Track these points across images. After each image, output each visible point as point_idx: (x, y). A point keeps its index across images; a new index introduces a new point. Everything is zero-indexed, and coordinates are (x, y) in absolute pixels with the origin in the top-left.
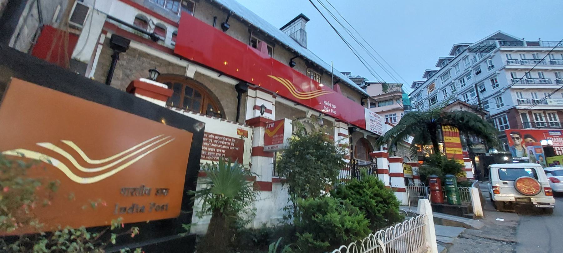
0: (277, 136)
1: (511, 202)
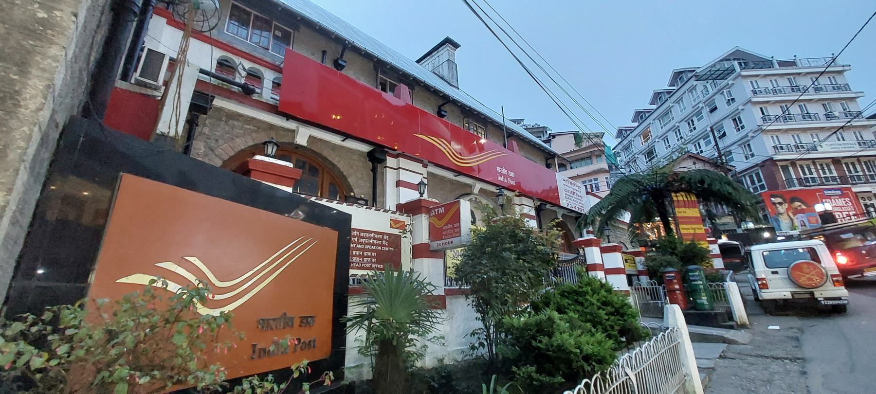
0: (450, 226)
1: (785, 300)
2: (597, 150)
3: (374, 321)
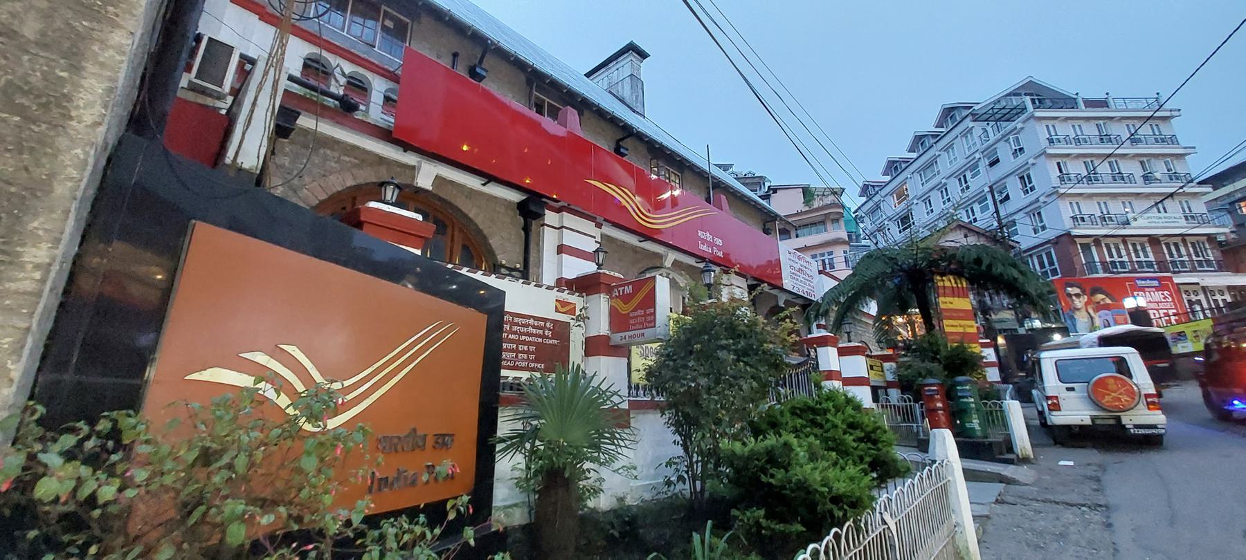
0: (640, 312)
2: (833, 214)
3: (538, 443)
